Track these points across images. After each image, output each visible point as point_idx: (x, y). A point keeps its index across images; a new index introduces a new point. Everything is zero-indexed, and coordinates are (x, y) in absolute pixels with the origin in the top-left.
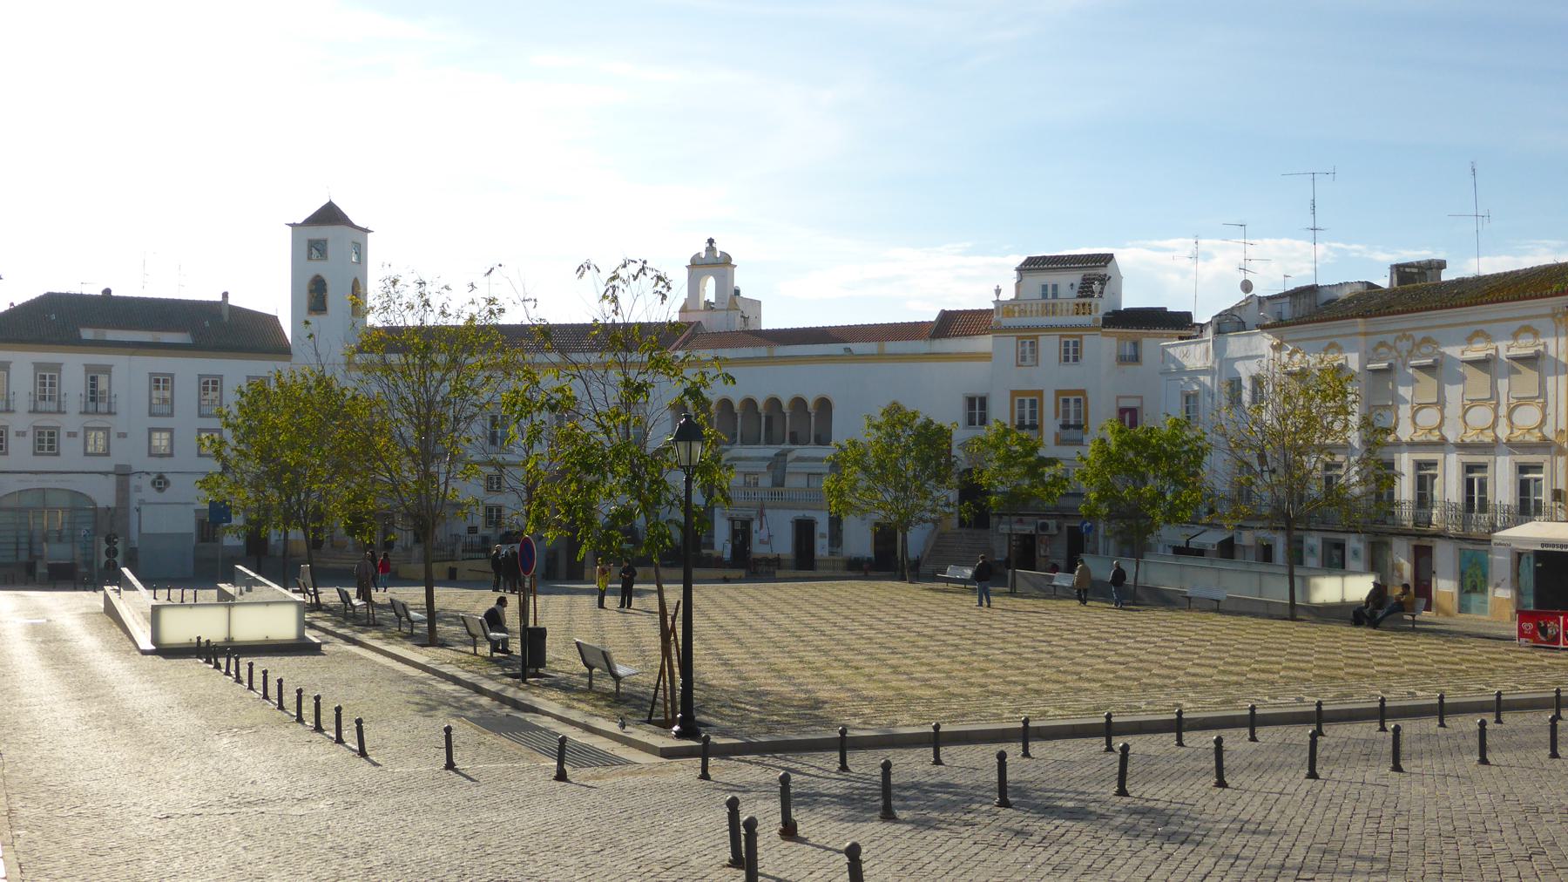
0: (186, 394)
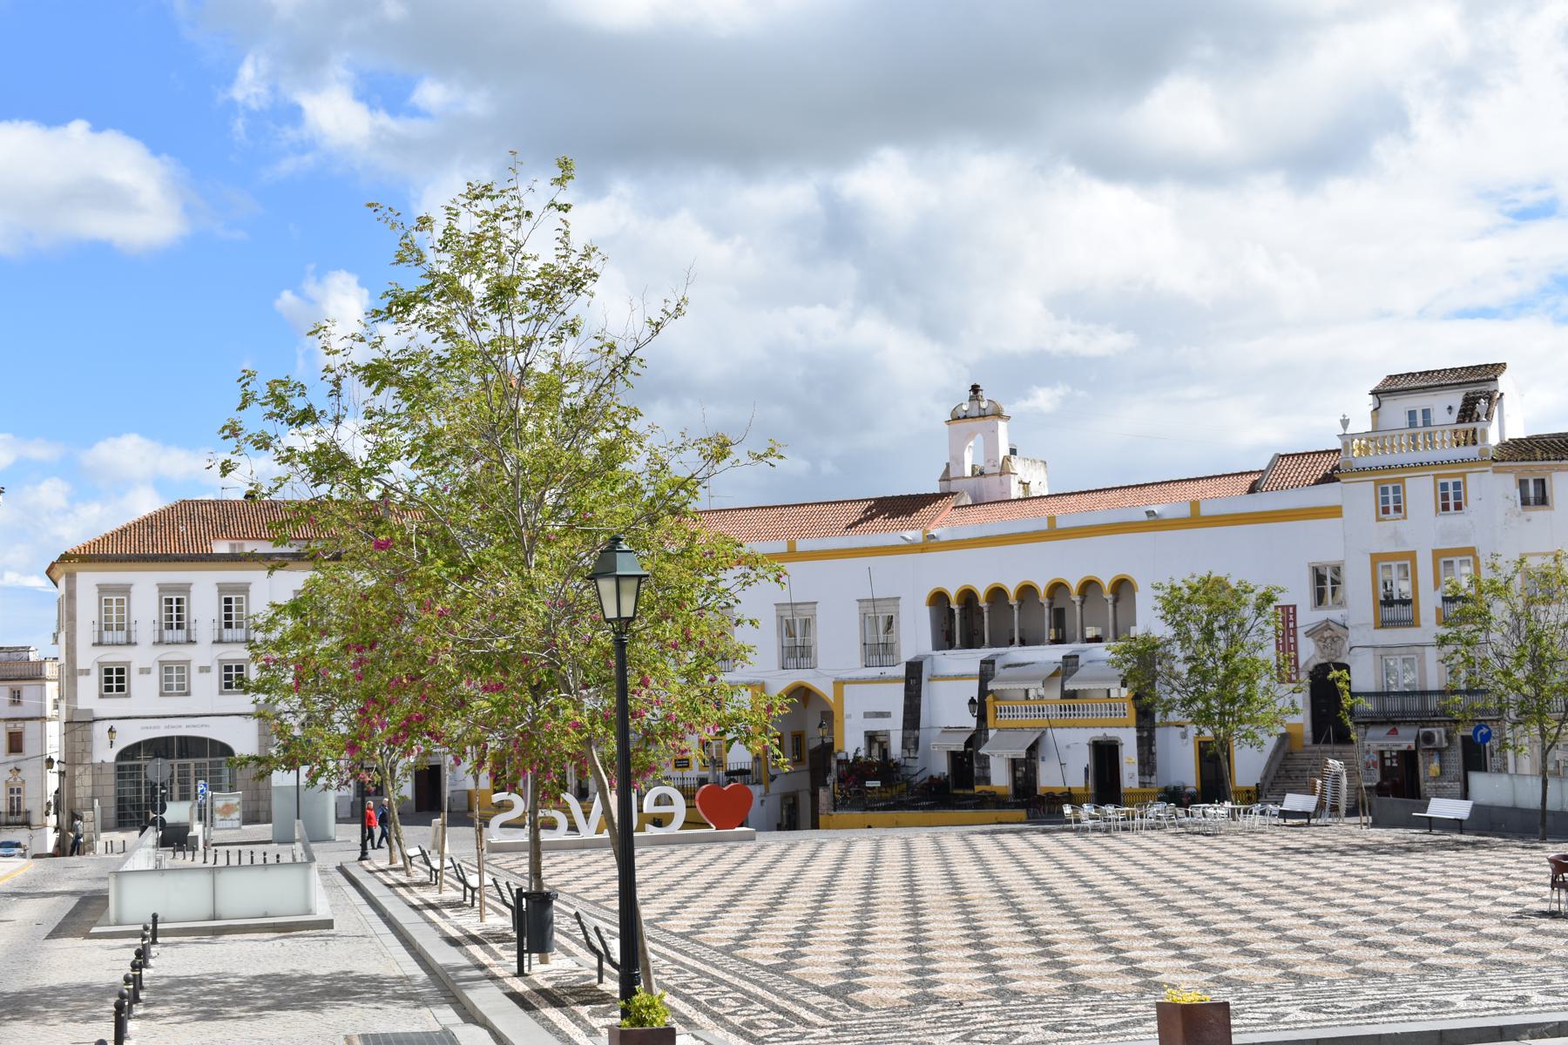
0: (204, 607)
